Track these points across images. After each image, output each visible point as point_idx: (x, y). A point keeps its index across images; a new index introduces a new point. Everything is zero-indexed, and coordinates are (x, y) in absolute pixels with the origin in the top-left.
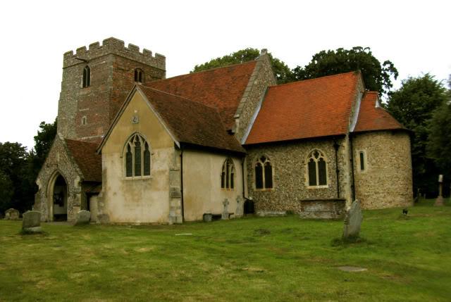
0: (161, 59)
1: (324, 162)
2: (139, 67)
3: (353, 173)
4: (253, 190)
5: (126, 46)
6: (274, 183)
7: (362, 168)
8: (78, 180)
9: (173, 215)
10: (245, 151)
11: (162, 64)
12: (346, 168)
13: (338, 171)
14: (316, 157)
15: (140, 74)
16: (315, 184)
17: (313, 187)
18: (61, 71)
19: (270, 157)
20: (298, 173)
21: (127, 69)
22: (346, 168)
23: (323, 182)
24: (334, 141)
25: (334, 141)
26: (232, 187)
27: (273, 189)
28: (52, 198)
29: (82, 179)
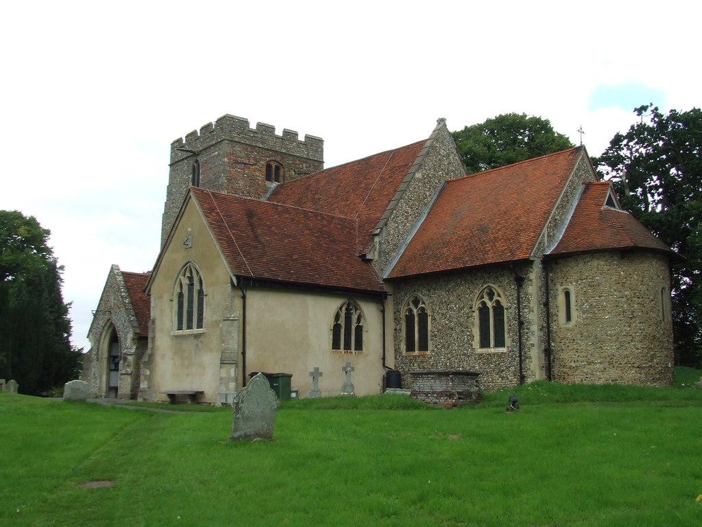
0: (315, 144)
1: (427, 314)
2: (273, 158)
3: (548, 327)
4: (401, 353)
5: (253, 126)
6: (430, 343)
7: (569, 318)
8: (130, 336)
9: (223, 389)
10: (387, 288)
11: (316, 151)
12: (533, 316)
13: (521, 324)
14: (491, 299)
15: (277, 168)
16: (488, 346)
17: (484, 350)
18: (166, 171)
19: (425, 298)
20: (464, 327)
21: (252, 161)
22: (533, 316)
23: (500, 342)
24: (516, 270)
25: (516, 270)
26: (359, 346)
27: (428, 353)
28: (105, 362)
29: (135, 334)
